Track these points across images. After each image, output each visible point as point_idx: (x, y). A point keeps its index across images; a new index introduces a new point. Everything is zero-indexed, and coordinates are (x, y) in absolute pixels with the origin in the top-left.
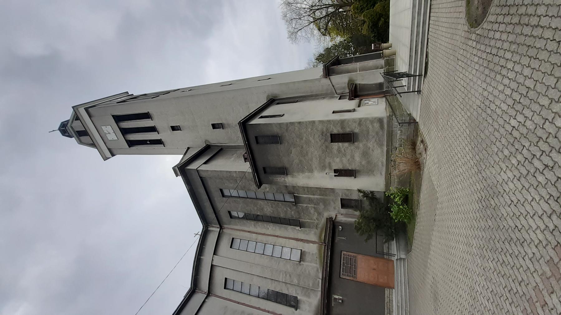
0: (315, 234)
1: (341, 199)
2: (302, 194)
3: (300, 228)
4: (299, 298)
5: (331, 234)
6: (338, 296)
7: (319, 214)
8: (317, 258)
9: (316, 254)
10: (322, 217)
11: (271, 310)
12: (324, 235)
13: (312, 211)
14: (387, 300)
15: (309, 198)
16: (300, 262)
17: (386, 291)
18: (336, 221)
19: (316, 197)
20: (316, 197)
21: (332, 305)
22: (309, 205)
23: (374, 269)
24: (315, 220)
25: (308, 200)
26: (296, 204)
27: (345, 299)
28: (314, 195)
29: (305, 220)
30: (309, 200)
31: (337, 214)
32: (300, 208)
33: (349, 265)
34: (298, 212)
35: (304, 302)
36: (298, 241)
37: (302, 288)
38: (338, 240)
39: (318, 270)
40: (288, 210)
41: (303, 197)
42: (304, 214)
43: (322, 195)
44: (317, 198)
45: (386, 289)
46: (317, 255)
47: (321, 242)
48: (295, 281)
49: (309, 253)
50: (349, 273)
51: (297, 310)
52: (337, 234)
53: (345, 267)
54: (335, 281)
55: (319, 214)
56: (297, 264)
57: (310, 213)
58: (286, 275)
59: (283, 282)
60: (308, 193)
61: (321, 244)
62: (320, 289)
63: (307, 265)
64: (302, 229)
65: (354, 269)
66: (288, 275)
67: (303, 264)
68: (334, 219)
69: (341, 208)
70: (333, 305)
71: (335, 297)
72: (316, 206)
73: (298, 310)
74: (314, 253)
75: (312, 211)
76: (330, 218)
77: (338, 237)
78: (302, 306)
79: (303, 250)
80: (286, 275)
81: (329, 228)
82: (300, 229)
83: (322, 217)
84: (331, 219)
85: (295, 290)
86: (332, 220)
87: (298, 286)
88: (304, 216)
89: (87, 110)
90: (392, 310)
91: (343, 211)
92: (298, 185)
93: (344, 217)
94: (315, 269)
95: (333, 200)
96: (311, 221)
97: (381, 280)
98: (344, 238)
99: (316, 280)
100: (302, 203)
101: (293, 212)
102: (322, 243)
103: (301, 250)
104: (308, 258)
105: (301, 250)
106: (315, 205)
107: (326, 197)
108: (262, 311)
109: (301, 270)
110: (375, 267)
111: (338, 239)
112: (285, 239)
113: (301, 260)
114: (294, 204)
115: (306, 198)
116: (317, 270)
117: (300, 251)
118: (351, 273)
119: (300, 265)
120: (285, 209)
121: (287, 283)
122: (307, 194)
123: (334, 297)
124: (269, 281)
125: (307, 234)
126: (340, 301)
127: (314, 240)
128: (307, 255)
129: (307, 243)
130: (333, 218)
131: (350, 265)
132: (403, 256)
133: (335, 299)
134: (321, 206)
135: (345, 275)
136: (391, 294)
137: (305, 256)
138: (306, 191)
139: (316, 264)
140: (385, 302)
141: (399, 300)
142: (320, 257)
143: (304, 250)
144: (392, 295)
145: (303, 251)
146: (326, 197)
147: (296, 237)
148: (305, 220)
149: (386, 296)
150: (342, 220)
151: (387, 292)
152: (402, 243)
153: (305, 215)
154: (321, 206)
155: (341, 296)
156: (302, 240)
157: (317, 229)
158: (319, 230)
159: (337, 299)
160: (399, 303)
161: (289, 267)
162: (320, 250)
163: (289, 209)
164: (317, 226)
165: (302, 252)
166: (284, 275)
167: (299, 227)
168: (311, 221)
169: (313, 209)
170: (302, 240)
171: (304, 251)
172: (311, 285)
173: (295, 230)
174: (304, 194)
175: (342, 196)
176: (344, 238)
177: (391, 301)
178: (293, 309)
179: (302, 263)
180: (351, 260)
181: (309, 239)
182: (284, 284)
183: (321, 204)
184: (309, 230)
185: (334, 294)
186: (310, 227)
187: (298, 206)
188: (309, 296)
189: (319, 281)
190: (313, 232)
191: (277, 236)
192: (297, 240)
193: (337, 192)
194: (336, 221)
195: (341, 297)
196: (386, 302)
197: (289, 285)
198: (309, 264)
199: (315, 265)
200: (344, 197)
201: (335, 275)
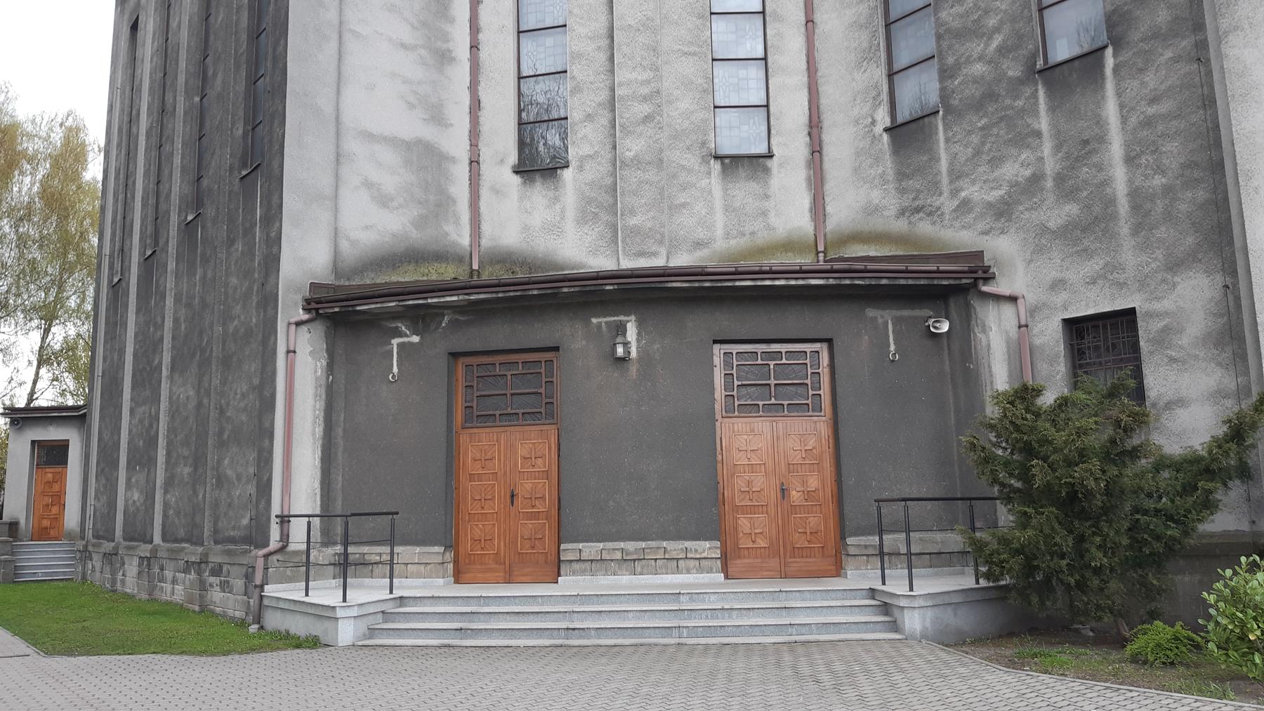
0: (872, 210)
1: (1133, 311)
2: (1119, 94)
3: (886, 130)
4: (567, 175)
5: (910, 282)
6: (638, 341)
7: (1002, 212)
8: (753, 233)
9: (769, 227)
10: (981, 226)
11: (483, 55)
12: (872, 254)
13: (1014, 170)
14: (674, 547)
15: (1102, 139)
16: (716, 157)
17: (707, 544)
18: (976, 304)
19: (1120, 175)
20: (1120, 175)
21: (597, 316)
22: (1047, 148)
23: (784, 492)
24: (954, 193)
25: (1086, 136)
26: (1040, 72)
27: (633, 370)
28: (1130, 160)
29: (942, 144)
30: (1086, 142)
31: (1020, 301)
32: (1020, 103)
33: (773, 382)
34: (990, 96)
35: (556, 199)
36: (809, 134)
37: (608, 181)
38: (880, 321)
39: (699, 245)
40: (990, 38)
41: (1100, 102)
42: (982, 129)
43: (1135, 207)
44: (1106, 182)
45: (718, 544)
46: (762, 238)
47: (825, 248)
48: (632, 147)
49: (767, 197)
50: (740, 383)
51: (516, 172)
52: (906, 313)
53: (759, 362)
54: (699, 323)
55: (1002, 212)
56: (704, 144)
57: (995, 162)
58: (645, 99)
59: (613, 90)
60: (1133, 120)
61: (821, 248)
62: (627, 264)
63: (710, 192)
64: (885, 137)
65: (761, 403)
66: (646, 109)
67: (709, 173)
68: (985, 289)
69: (1065, 321)
70: (594, 320)
71: (629, 325)
72: (1049, 184)
73: (517, 180)
74: (773, 220)
75: (1014, 170)
76: (986, 270)
77: (897, 321)
78: (539, 193)
79: (773, 164)
80: (645, 99)
81: (938, 272)
82: (879, 129)
83: (981, 226)
84: (980, 274)
85: (591, 153)
86: (976, 279)
87: (614, 165)
88: (970, 133)
89: (57, 518)
90: (639, 569)
91: (1049, 334)
92: (1231, 37)
93: (1008, 342)
94: (701, 234)
95: (1112, 268)
96: (945, 180)
97: (744, 523)
98: (892, 348)
99: (661, 242)
100: (1052, 109)
101: (979, 68)
102: (825, 252)
103: (770, 156)
104: (744, 190)
105: (770, 156)
106: (1060, 179)
107: (1124, 229)
108: (468, 16)
109: (683, 167)
110: (795, 496)
111: (886, 318)
112: (804, 65)
113: (727, 161)
114: (1040, 64)
115: (1100, 122)
116: (698, 244)
117: (761, 149)
118: (744, 391)
119: (704, 160)
120: (992, 22)
121: (613, 110)
122: (1124, 120)
123: (628, 321)
124: (600, 24)
125: (856, 170)
126: (620, 351)
127: (829, 209)
128: (753, 186)
129: (809, 180)
130: (991, 282)
131: (776, 385)
132: (914, 621)
133: (621, 329)
134: (1058, 214)
135: (728, 364)
136: (701, 563)
137: (750, 178)
138: (1151, 111)
139: (727, 235)
140: (666, 540)
141: (703, 601)
142: (762, 251)
143: (775, 170)
144: (700, 570)
145: (769, 163)
146: (1124, 229)
147: (828, 119)
148: (942, 144)
149: (688, 544)
150: (984, 330)
151: (708, 548)
152: (964, 620)
153: (975, 139)
154: (1058, 214)
155: (638, 352)
156: (816, 149)
157: (902, 213)
158: (900, 226)
159: (624, 334)
160: (692, 600)
161: (685, 104)
162: (788, 245)
163: (995, 44)
164: (918, 210)
165: (761, 160)
166: (645, 90)
167: (888, 123)
168: (945, 180)
169: (1028, 173)
170: (816, 149)
171: (767, 170)
172: (633, 221)
173: (866, 108)
174: (1122, 106)
175: (1150, 315)
176: (892, 348)
177: (674, 563)
178: (513, 158)
179: (716, 166)
180: (801, 390)
181: (830, 187)
182: (604, 96)
183: (1072, 209)
184: (882, 176)
185: (641, 325)
186: (901, 176)
187: (1028, 91)
188: (585, 217)
189: (655, 254)
190: (876, 196)
191: (810, 21)
192: (815, 126)
193: (1174, 285)
194: (976, 304)
195: (634, 354)
196: (665, 544)
197: (604, 121)
198: (718, 204)
199: (719, 232)
200: (1146, 331)
201: (725, 321)
